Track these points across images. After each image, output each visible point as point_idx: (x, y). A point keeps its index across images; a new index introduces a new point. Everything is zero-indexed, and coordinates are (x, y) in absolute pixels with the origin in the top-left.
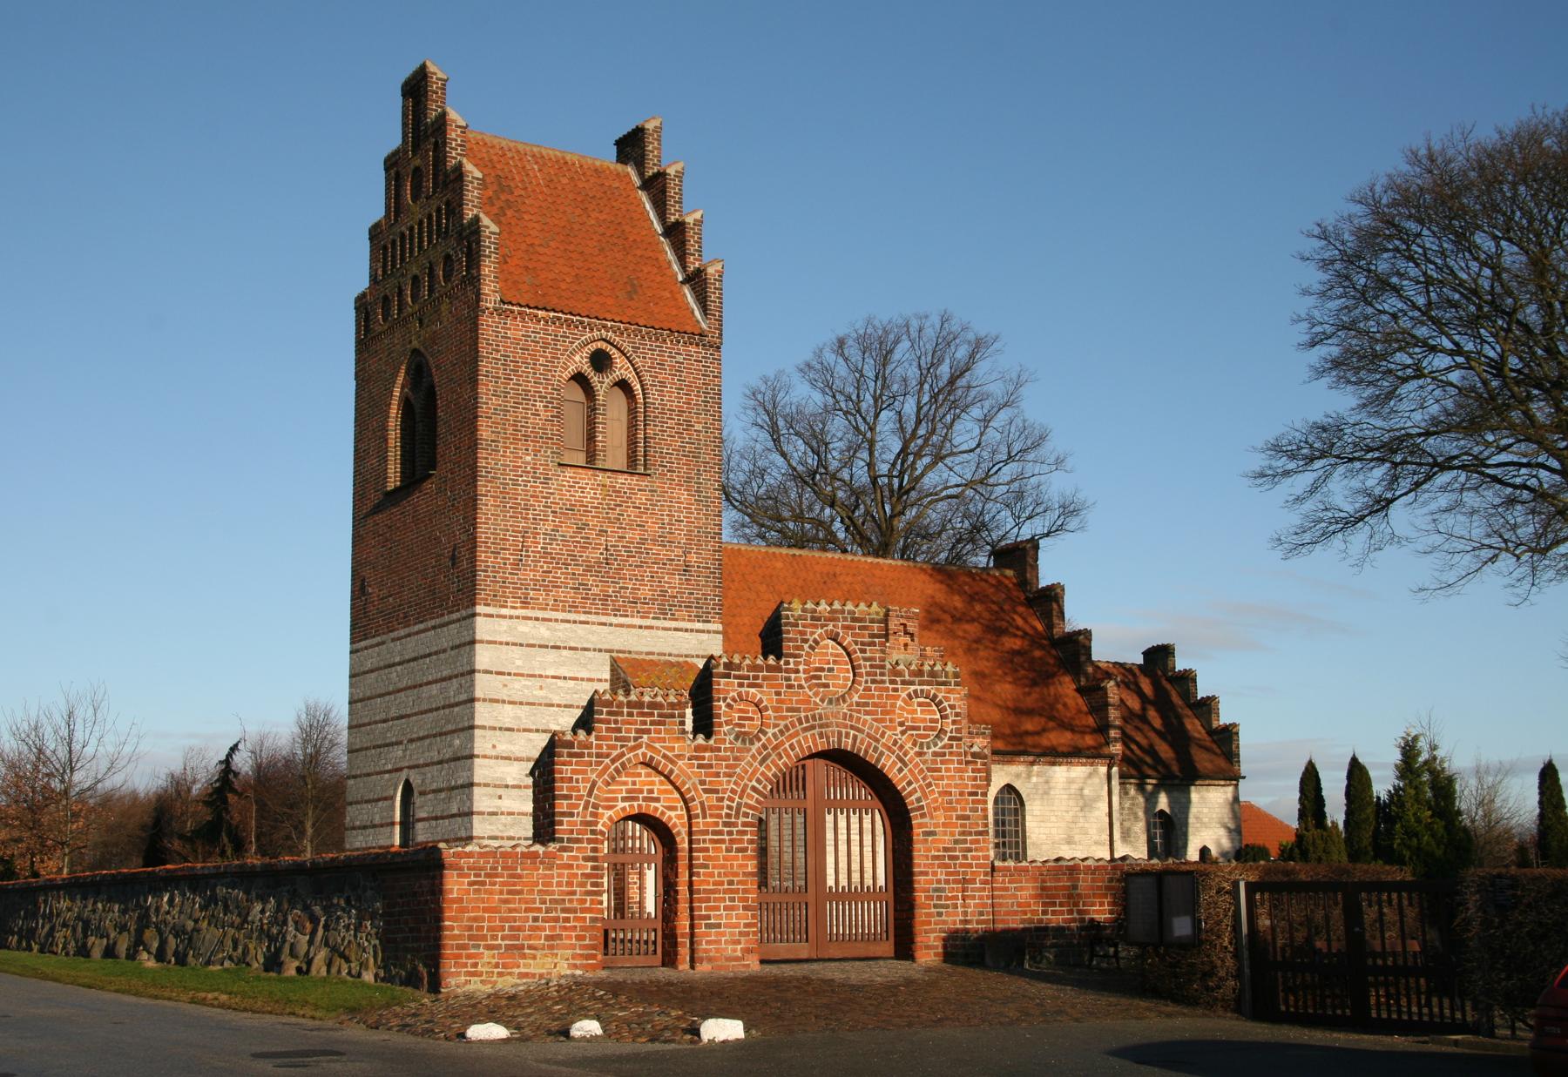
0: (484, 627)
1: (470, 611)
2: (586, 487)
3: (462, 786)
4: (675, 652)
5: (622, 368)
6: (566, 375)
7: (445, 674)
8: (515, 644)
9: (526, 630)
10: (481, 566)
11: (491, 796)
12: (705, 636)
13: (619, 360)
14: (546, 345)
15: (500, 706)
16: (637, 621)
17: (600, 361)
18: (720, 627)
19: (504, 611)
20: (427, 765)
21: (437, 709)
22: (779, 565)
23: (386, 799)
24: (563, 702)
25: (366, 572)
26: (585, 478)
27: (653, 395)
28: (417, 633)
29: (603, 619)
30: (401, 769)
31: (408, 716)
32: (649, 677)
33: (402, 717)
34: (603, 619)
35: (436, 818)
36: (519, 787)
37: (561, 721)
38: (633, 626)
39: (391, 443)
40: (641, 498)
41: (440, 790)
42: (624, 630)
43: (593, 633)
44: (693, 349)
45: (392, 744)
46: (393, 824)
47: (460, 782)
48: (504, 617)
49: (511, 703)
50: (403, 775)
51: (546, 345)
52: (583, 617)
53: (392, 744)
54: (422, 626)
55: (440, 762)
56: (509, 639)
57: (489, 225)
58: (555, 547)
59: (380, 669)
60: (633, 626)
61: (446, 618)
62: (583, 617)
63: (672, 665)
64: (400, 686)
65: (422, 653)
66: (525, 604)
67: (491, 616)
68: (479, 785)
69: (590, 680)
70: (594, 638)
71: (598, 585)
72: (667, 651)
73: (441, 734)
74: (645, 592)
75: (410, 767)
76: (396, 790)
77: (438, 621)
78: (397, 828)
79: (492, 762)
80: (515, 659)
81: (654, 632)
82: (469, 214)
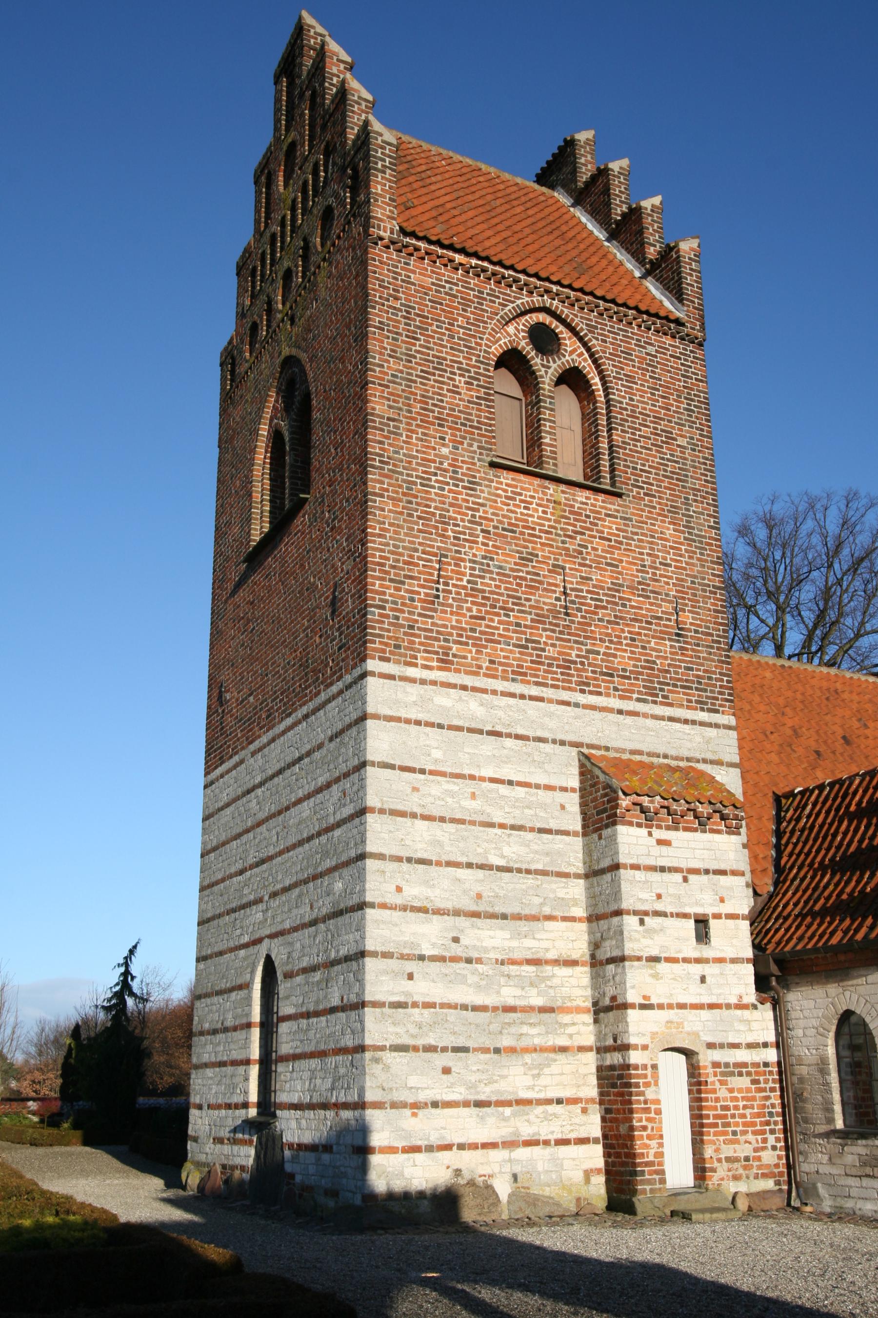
0: (378, 694)
1: (357, 672)
2: (534, 501)
3: (347, 959)
4: (672, 752)
5: (571, 353)
6: (496, 350)
7: (321, 781)
8: (432, 725)
9: (447, 703)
10: (374, 599)
11: (395, 974)
12: (712, 732)
13: (569, 342)
14: (466, 303)
15: (408, 821)
16: (615, 703)
17: (544, 339)
18: (732, 721)
19: (411, 672)
20: (295, 929)
21: (310, 839)
22: (768, 674)
23: (240, 987)
24: (509, 821)
25: (226, 675)
26: (529, 486)
27: (619, 393)
28: (284, 733)
29: (565, 695)
30: (259, 941)
31: (270, 858)
32: (643, 781)
33: (263, 862)
34: (565, 695)
35: (308, 1015)
36: (442, 959)
37: (507, 850)
38: (610, 710)
39: (257, 497)
40: (610, 527)
41: (313, 969)
42: (597, 715)
43: (551, 715)
44: (668, 340)
45: (249, 905)
46: (249, 1025)
47: (343, 952)
48: (413, 681)
49: (425, 818)
50: (262, 950)
51: (466, 303)
52: (535, 691)
53: (249, 905)
54: (289, 721)
55: (314, 923)
56: (421, 716)
57: (384, 135)
58: (488, 583)
59: (238, 798)
60: (610, 710)
61: (323, 697)
62: (535, 691)
63: (674, 770)
64: (261, 816)
65: (289, 759)
66: (445, 663)
67: (392, 677)
68: (374, 954)
69: (549, 788)
70: (552, 724)
71: (558, 647)
72: (661, 750)
73: (315, 877)
74: (623, 660)
75: (272, 936)
76: (253, 972)
77: (311, 705)
78: (256, 1033)
79: (397, 915)
80: (432, 748)
81: (640, 720)
82: (355, 120)
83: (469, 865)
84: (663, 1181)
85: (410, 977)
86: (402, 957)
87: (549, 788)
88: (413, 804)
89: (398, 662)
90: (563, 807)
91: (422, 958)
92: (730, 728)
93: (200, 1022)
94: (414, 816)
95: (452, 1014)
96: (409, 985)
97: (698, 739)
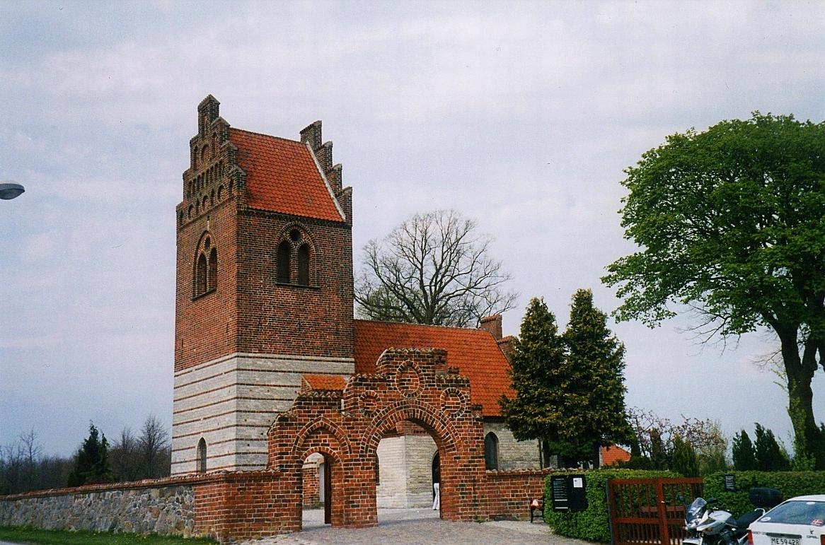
8: (256, 370)
11: (244, 445)
18: (353, 360)
19: (250, 355)
29: (298, 357)
30: (200, 433)
36: (258, 440)
48: (250, 357)
52: (288, 357)
62: (288, 357)
66: (261, 351)
67: (244, 357)
79: (245, 428)
81: (322, 363)
83: (267, 412)
84: (319, 500)
85: (249, 445)
86: (246, 440)
87: (292, 386)
88: (251, 395)
89: (246, 352)
90: (296, 392)
91: (252, 440)
92: (352, 362)
93: (176, 458)
94: (250, 398)
95: (260, 455)
96: (248, 448)
97: (341, 366)
